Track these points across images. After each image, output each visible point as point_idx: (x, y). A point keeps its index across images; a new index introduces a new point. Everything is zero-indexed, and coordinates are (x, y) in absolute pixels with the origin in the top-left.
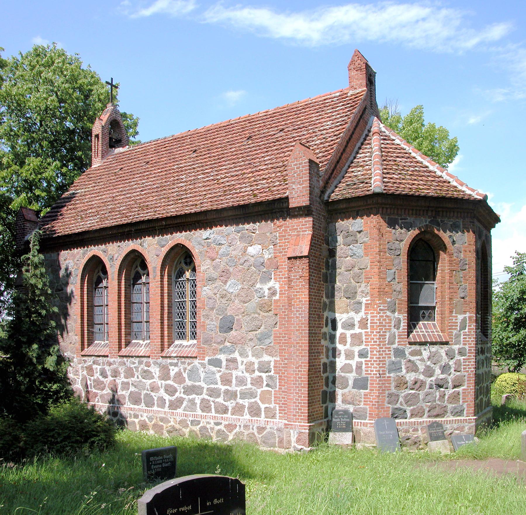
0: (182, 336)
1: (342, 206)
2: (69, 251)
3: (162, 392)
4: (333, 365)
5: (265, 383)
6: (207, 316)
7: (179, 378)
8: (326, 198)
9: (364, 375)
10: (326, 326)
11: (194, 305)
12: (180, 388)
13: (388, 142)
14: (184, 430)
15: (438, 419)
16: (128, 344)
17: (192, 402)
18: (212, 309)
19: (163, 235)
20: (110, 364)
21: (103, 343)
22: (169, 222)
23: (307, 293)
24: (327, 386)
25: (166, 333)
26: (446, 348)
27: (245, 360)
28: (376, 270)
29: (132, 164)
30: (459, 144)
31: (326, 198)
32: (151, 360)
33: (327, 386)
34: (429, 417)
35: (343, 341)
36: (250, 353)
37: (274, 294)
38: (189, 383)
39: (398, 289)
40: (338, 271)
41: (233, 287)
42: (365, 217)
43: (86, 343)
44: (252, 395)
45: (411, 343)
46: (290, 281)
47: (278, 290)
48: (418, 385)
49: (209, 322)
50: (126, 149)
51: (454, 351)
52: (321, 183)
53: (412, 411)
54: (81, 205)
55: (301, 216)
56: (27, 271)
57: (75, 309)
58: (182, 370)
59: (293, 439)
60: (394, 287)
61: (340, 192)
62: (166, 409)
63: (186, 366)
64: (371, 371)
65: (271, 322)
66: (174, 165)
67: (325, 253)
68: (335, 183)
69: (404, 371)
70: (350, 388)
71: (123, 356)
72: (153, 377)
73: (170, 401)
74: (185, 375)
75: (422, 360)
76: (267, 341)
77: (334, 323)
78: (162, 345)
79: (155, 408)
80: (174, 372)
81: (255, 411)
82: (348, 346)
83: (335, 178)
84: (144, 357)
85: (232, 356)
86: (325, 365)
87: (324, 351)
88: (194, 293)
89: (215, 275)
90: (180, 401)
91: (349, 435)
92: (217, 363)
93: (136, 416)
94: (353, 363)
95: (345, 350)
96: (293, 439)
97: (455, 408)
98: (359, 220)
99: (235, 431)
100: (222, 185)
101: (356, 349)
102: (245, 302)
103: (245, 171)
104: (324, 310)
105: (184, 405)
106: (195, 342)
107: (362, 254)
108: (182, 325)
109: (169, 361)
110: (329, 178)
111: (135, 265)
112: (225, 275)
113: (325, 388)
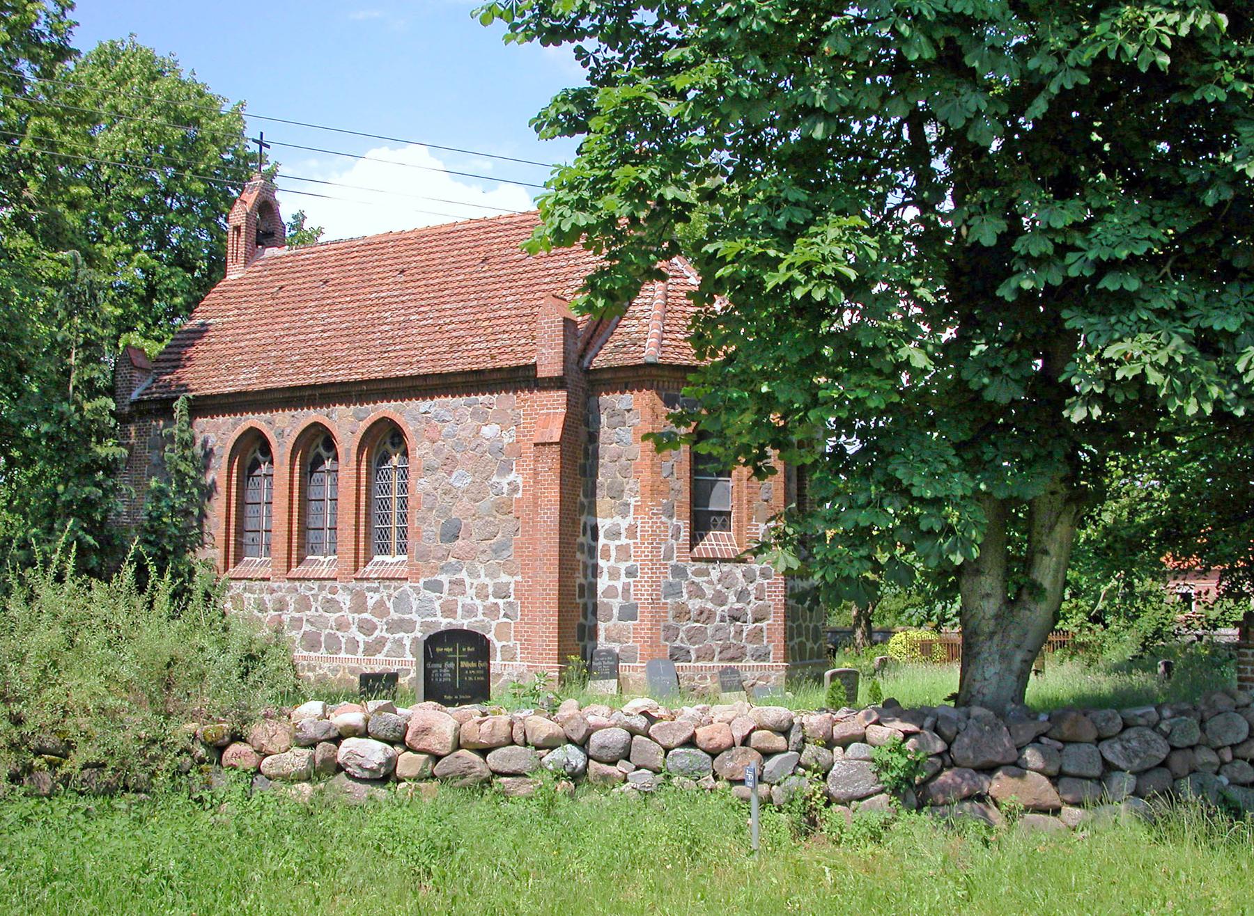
0: (385, 550)
1: (606, 376)
2: (209, 419)
4: (593, 587)
5: (502, 613)
6: (423, 520)
8: (586, 364)
9: (632, 600)
10: (584, 534)
11: (404, 503)
12: (381, 624)
13: (679, 281)
15: (733, 664)
16: (300, 561)
17: (399, 643)
18: (431, 509)
19: (362, 405)
20: (272, 591)
21: (258, 560)
22: (372, 387)
23: (558, 490)
24: (585, 617)
25: (362, 544)
26: (743, 567)
27: (476, 582)
28: (649, 462)
29: (301, 281)
31: (586, 364)
32: (337, 584)
33: (585, 617)
34: (721, 660)
35: (607, 556)
36: (482, 573)
37: (515, 490)
38: (394, 615)
39: (677, 487)
40: (601, 461)
41: (461, 480)
42: (635, 392)
43: (231, 561)
45: (694, 560)
46: (536, 473)
47: (521, 486)
48: (705, 616)
49: (425, 528)
50: (284, 251)
51: (754, 571)
52: (579, 345)
53: (697, 650)
54: (220, 346)
55: (552, 388)
56: (172, 451)
57: (217, 509)
58: (385, 598)
60: (672, 485)
61: (602, 359)
62: (360, 655)
63: (392, 591)
64: (642, 595)
65: (511, 527)
66: (370, 293)
67: (583, 437)
68: (599, 343)
69: (686, 596)
70: (615, 619)
71: (294, 579)
74: (390, 605)
75: (710, 582)
76: (506, 553)
77: (595, 530)
78: (357, 561)
79: (343, 655)
80: (373, 601)
83: (600, 336)
84: (329, 579)
85: (458, 576)
86: (582, 587)
87: (581, 567)
88: (404, 488)
89: (436, 462)
90: (381, 642)
91: (613, 683)
92: (436, 586)
93: (312, 669)
94: (619, 585)
97: (757, 650)
98: (628, 395)
100: (447, 335)
101: (623, 566)
103: (478, 316)
104: (581, 513)
105: (386, 649)
106: (404, 557)
108: (385, 534)
109: (366, 584)
110: (592, 337)
111: (317, 444)
112: (450, 463)
113: (582, 620)
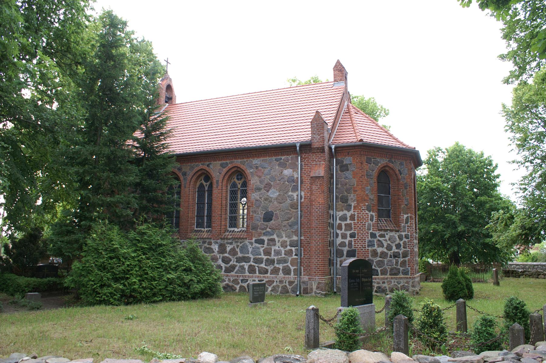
3: (220, 262)
5: (294, 253)
7: (233, 252)
9: (353, 248)
14: (235, 286)
26: (398, 234)
27: (281, 240)
30: (120, 14)
36: (284, 235)
38: (240, 255)
41: (273, 194)
44: (285, 261)
58: (236, 247)
59: (314, 287)
63: (239, 244)
69: (376, 246)
72: (214, 252)
73: (225, 267)
74: (238, 250)
76: (296, 227)
81: (287, 271)
82: (343, 231)
85: (272, 237)
90: (233, 267)
92: (261, 242)
94: (347, 241)
95: (341, 234)
96: (314, 287)
99: (273, 285)
101: (348, 233)
102: (280, 203)
107: (351, 177)
112: (268, 187)
